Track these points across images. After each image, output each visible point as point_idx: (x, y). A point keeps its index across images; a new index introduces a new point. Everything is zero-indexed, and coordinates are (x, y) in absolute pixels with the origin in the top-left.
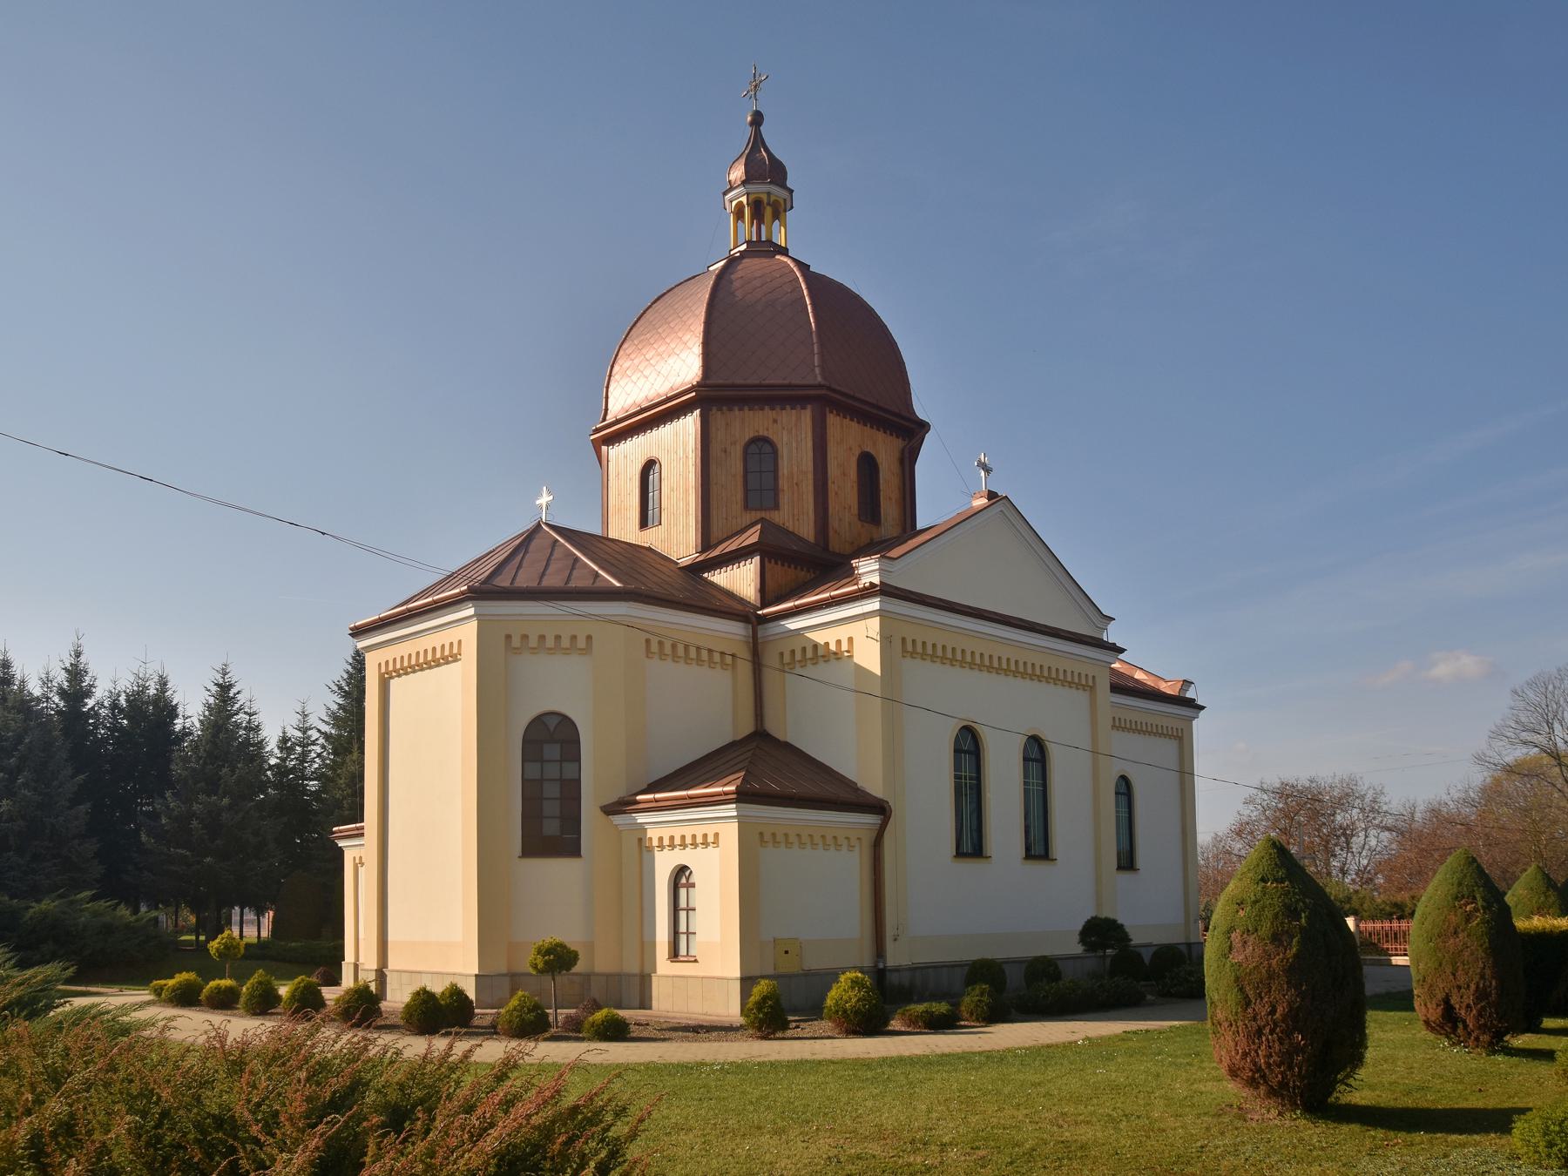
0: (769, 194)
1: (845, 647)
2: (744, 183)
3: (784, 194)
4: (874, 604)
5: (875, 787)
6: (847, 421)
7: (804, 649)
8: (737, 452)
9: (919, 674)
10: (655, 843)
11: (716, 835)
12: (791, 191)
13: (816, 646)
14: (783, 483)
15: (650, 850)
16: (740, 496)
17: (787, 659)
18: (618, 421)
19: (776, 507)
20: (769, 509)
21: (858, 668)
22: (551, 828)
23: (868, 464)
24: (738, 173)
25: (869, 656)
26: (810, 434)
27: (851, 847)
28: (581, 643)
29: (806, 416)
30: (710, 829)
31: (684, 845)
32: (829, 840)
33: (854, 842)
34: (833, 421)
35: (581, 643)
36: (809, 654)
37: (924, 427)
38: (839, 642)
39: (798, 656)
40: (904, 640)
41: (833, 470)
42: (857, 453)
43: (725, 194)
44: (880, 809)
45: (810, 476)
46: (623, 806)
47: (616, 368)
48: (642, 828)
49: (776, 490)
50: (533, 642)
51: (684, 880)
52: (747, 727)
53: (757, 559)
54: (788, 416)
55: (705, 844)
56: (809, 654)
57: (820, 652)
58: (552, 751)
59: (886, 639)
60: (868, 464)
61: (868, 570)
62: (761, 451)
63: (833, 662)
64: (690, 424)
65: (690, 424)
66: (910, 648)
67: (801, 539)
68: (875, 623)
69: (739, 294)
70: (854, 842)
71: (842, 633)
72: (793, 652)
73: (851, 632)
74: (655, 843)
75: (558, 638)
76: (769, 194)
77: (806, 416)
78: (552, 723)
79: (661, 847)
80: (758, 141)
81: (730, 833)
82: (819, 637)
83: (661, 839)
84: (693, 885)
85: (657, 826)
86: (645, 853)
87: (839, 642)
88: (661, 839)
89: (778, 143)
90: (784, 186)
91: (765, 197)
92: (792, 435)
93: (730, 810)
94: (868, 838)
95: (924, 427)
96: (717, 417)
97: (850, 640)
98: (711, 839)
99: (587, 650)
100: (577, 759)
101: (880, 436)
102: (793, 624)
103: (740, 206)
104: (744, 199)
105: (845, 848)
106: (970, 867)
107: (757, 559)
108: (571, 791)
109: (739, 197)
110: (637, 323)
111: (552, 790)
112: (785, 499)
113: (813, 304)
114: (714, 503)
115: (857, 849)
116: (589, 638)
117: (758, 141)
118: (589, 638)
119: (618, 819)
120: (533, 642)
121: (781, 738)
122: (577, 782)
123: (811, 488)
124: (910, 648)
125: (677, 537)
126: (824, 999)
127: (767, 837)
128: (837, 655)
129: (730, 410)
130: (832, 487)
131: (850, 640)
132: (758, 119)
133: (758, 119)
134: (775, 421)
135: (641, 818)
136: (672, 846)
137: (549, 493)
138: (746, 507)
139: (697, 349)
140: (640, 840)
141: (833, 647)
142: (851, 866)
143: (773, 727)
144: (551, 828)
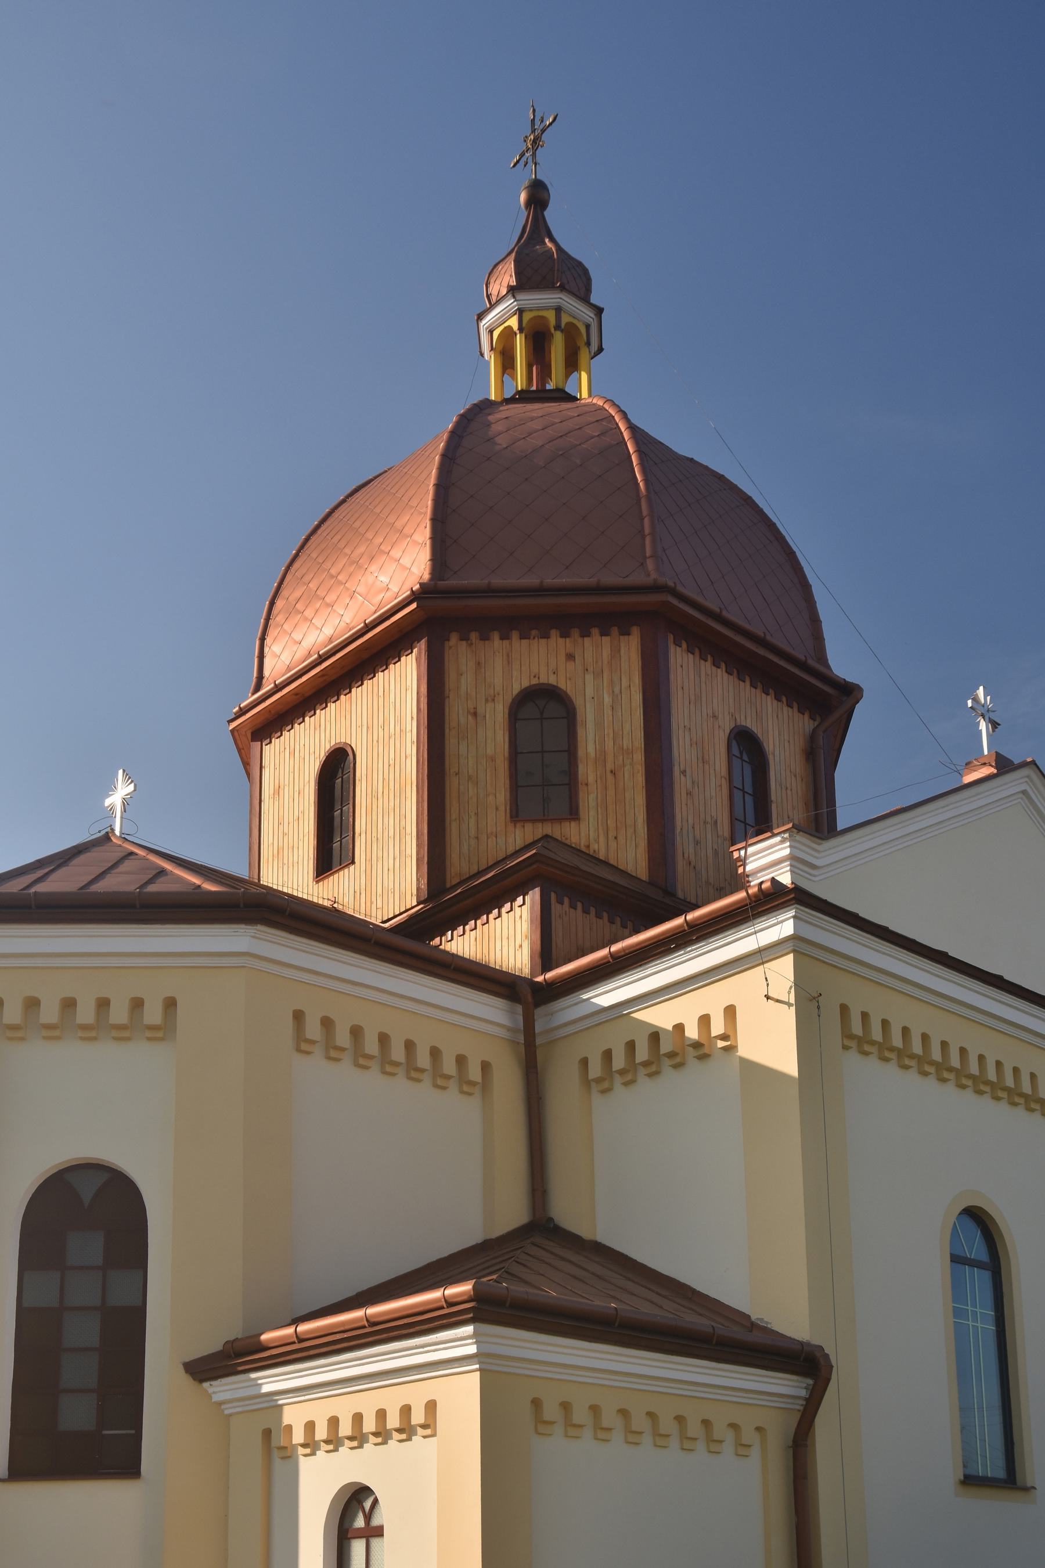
0: (558, 310)
1: (717, 1027)
2: (512, 290)
3: (586, 314)
4: (781, 926)
5: (792, 1319)
6: (707, 666)
7: (631, 1046)
8: (497, 714)
9: (879, 1089)
10: (298, 1437)
11: (431, 1407)
12: (599, 311)
13: (655, 1036)
14: (587, 772)
15: (288, 1455)
16: (502, 796)
17: (595, 1070)
18: (278, 688)
19: (573, 813)
20: (561, 820)
21: (749, 1067)
22: (77, 1414)
23: (746, 744)
24: (507, 276)
25: (771, 1039)
26: (637, 680)
27: (742, 1448)
28: (153, 1014)
29: (631, 648)
30: (415, 1394)
31: (359, 1438)
32: (694, 1428)
33: (749, 1435)
34: (684, 667)
35: (153, 1014)
36: (642, 1054)
37: (850, 692)
38: (705, 1021)
39: (619, 1061)
40: (844, 1009)
41: (683, 750)
42: (727, 726)
43: (480, 317)
44: (807, 1363)
45: (639, 757)
46: (239, 1356)
47: (279, 603)
48: (271, 1405)
49: (571, 782)
50: (50, 1013)
51: (360, 1522)
52: (512, 1213)
53: (534, 896)
54: (595, 648)
55: (407, 1430)
56: (642, 1054)
57: (665, 1047)
58: (86, 1248)
59: (809, 1002)
60: (746, 744)
61: (768, 859)
62: (543, 710)
63: (693, 1064)
64: (403, 681)
65: (403, 681)
66: (857, 1029)
67: (624, 873)
68: (784, 967)
69: (502, 441)
70: (749, 1435)
71: (710, 1000)
72: (608, 1055)
73: (738, 997)
74: (298, 1437)
75: (103, 1004)
76: (558, 310)
77: (631, 648)
78: (87, 1189)
79: (311, 1445)
80: (537, 227)
81: (461, 1398)
82: (660, 1016)
83: (310, 1427)
84: (379, 1532)
85: (302, 1394)
86: (278, 1463)
87: (705, 1021)
88: (310, 1427)
89: (569, 231)
90: (585, 299)
91: (551, 316)
92: (602, 682)
93: (460, 1341)
94: (779, 1429)
95: (850, 692)
96: (461, 655)
97: (730, 1011)
98: (418, 1417)
99: (165, 1030)
100: (138, 1260)
101: (769, 704)
102: (607, 995)
103: (508, 333)
104: (513, 323)
105: (728, 1448)
106: (993, 1509)
107: (534, 896)
108: (126, 1330)
109: (503, 316)
110: (326, 529)
111: (83, 1331)
112: (589, 800)
113: (642, 464)
114: (452, 785)
115: (755, 1452)
116: (170, 1004)
117: (537, 227)
118: (170, 1004)
119: (223, 1389)
120: (50, 1013)
121: (585, 1233)
122: (139, 1314)
123: (640, 779)
124: (857, 1029)
125: (384, 881)
126: (261, 1334)
127: (552, 1411)
128: (701, 1050)
129: (485, 638)
130: (681, 784)
131: (730, 1011)
132: (538, 196)
133: (538, 196)
134: (570, 657)
135: (271, 1382)
136: (334, 1442)
137: (129, 777)
138: (516, 815)
139: (423, 534)
140: (267, 1433)
141: (692, 1033)
142: (743, 1488)
143: (567, 1212)
144: (77, 1414)
